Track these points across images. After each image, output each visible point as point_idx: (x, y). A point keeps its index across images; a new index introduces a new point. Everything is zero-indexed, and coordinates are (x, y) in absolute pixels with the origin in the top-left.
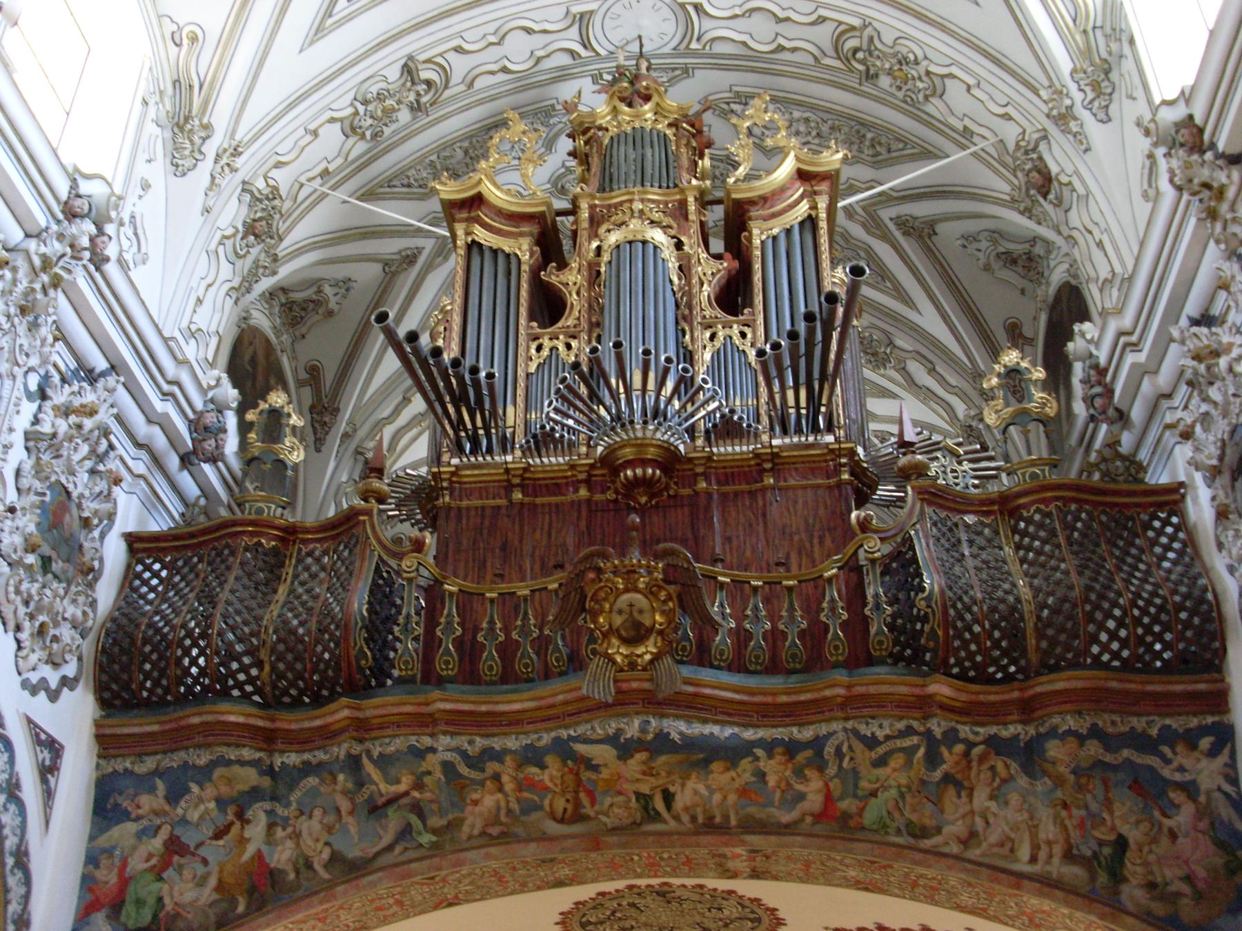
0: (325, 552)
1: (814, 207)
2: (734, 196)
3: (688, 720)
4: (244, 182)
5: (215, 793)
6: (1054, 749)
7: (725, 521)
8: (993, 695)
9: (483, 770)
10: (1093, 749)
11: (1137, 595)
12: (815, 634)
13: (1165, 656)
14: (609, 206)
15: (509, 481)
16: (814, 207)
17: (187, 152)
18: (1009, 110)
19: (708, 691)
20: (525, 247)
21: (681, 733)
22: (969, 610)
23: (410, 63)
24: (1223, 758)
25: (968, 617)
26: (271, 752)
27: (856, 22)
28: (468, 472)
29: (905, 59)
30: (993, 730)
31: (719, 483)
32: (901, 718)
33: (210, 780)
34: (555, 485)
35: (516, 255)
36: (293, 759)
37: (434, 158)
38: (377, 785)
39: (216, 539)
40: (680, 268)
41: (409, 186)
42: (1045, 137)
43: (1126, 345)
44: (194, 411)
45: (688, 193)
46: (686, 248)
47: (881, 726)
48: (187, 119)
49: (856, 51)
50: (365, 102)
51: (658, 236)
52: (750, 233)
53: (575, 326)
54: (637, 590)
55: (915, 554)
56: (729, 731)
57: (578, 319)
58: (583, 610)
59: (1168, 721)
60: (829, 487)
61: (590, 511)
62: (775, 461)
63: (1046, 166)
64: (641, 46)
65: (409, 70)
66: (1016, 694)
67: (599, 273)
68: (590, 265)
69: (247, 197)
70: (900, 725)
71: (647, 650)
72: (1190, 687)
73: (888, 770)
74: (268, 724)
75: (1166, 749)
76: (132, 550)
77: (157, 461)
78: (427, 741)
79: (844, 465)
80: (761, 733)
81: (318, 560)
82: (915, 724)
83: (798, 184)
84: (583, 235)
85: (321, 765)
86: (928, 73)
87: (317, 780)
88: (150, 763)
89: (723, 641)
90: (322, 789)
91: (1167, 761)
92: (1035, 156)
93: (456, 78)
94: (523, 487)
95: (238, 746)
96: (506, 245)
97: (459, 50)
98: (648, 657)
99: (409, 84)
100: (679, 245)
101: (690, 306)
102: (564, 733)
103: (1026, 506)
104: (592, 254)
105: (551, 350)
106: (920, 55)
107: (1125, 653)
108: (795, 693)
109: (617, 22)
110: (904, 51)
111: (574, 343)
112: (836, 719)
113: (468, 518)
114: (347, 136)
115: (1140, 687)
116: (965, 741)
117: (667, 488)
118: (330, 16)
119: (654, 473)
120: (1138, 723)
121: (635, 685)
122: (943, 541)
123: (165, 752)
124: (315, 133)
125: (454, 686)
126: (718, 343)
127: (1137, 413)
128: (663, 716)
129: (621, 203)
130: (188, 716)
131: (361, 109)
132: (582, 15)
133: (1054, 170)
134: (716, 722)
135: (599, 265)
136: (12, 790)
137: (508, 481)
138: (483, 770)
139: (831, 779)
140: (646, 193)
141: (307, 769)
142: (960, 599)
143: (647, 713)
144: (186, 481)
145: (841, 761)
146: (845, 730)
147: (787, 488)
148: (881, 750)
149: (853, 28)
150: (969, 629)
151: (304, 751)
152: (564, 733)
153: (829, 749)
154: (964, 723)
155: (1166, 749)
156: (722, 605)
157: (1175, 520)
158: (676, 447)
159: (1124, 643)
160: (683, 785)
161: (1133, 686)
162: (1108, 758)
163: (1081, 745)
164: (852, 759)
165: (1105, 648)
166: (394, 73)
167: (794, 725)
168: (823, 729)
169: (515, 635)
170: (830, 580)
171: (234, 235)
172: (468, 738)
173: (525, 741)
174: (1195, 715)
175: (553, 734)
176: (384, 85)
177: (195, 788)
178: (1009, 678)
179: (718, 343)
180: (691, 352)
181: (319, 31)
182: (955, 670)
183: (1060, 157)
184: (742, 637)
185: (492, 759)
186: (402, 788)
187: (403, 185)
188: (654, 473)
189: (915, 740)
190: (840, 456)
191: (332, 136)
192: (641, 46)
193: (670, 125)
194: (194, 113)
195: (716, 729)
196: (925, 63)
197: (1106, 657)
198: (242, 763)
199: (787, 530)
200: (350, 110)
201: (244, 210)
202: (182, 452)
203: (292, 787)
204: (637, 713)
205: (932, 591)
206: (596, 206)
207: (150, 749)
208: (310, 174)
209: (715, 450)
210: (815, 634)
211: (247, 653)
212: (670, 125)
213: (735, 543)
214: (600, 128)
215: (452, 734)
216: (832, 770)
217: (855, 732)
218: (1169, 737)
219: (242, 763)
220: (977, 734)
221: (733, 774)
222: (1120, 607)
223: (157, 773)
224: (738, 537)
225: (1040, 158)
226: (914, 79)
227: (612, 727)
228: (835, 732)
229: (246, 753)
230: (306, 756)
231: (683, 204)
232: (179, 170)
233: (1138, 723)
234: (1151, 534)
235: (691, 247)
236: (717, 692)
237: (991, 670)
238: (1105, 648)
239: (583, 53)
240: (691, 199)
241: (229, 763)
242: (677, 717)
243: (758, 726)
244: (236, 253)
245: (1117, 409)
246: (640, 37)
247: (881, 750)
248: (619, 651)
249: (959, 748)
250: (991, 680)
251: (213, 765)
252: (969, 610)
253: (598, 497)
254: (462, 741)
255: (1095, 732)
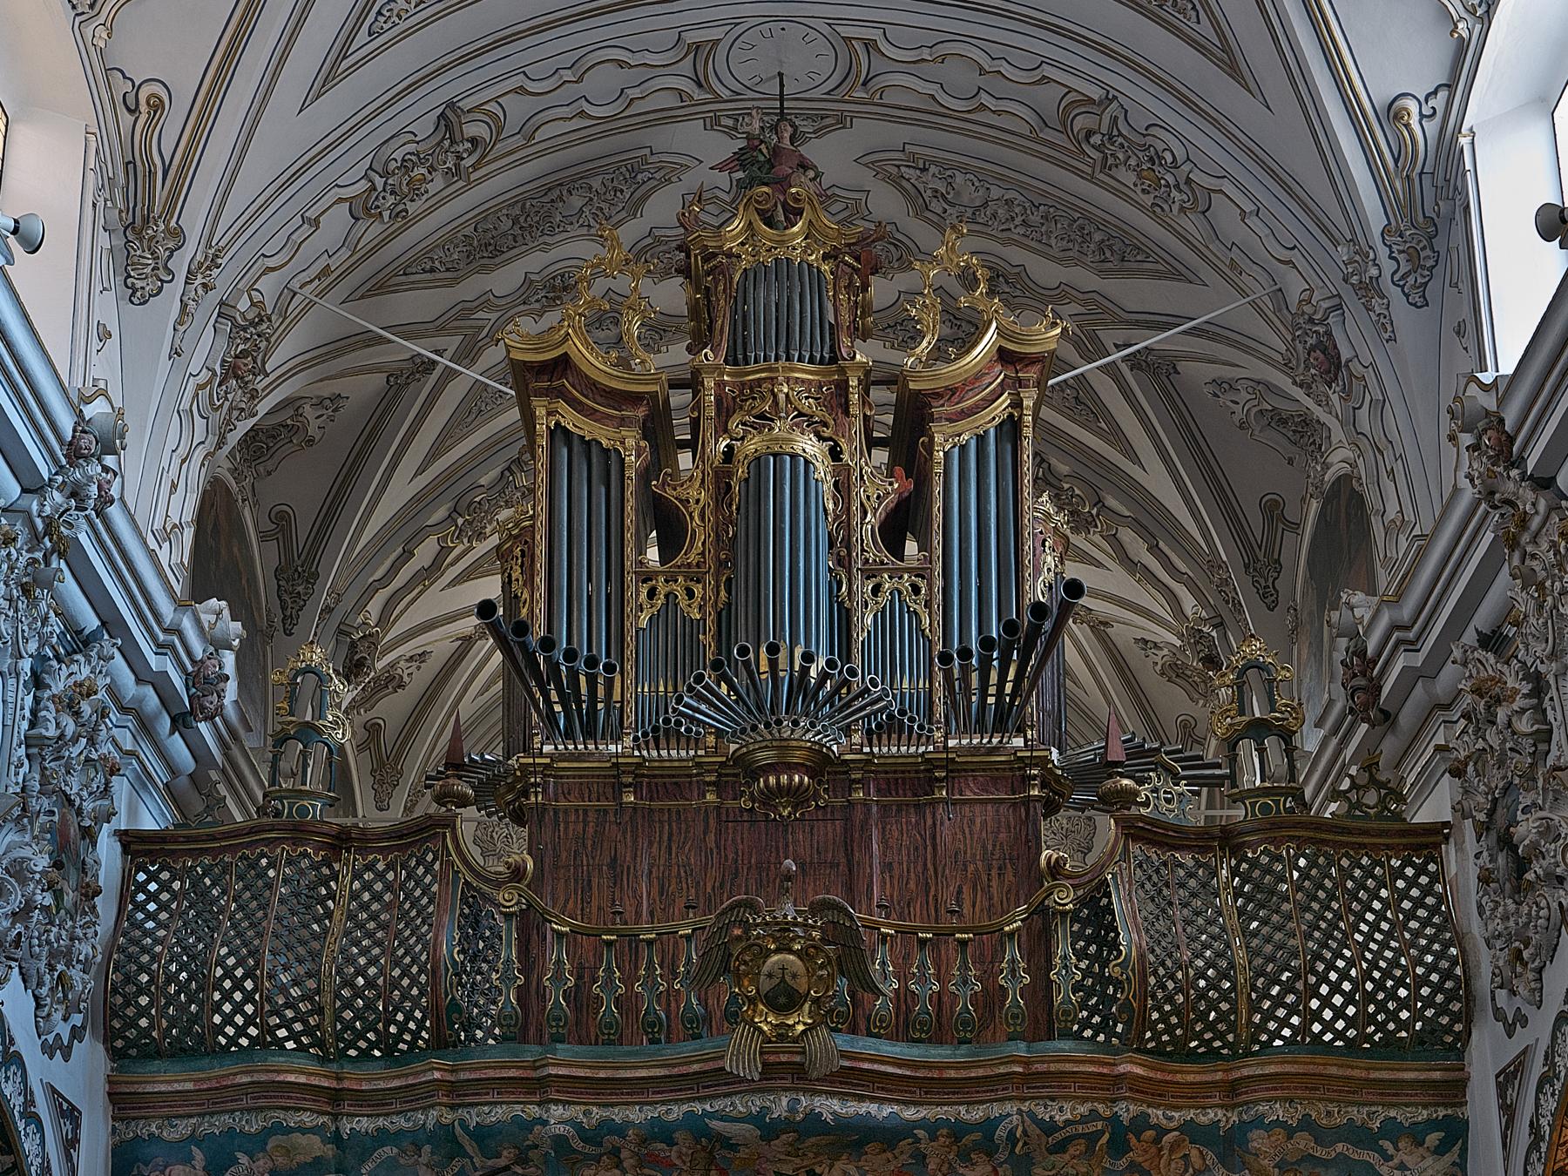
0: (390, 867)
1: (1017, 404)
2: (912, 386)
3: (843, 1097)
4: (222, 303)
5: (270, 1164)
6: (1258, 1140)
7: (884, 842)
8: (1191, 1075)
9: (600, 1144)
10: (1303, 1141)
11: (1374, 965)
12: (991, 999)
13: (1376, 1038)
14: (743, 384)
15: (616, 775)
16: (1017, 404)
17: (148, 270)
18: (1295, 256)
19: (866, 1066)
20: (630, 442)
21: (834, 1113)
22: (1172, 977)
23: (449, 113)
24: (1453, 1155)
25: (1170, 985)
26: (336, 1117)
27: (1096, 93)
28: (565, 765)
29: (1161, 158)
30: (1191, 1114)
31: (879, 791)
32: (1084, 1100)
33: (264, 1150)
34: (670, 783)
35: (616, 450)
36: (365, 1124)
37: (469, 231)
38: (471, 1158)
39: (248, 845)
40: (836, 484)
41: (432, 270)
42: (1339, 307)
43: (1407, 628)
44: (193, 662)
45: (849, 373)
46: (845, 457)
47: (1061, 1109)
48: (146, 220)
49: (1089, 134)
50: (386, 174)
51: (809, 446)
52: (932, 439)
53: (698, 565)
54: (791, 951)
55: (1110, 903)
56: (887, 1110)
57: (703, 553)
58: (726, 970)
59: (1392, 1113)
60: (1014, 805)
61: (719, 821)
62: (953, 768)
63: (1335, 347)
64: (782, 85)
65: (448, 119)
66: (1219, 1076)
67: (729, 486)
68: (716, 472)
69: (227, 326)
70: (1083, 1109)
71: (799, 1022)
72: (1423, 1076)
73: (1067, 1157)
74: (334, 1084)
75: (1387, 1145)
76: (126, 849)
77: (145, 727)
78: (534, 1111)
79: (1034, 777)
80: (923, 1112)
81: (381, 876)
82: (1100, 1107)
83: (998, 368)
84: (708, 428)
85: (400, 1133)
86: (1189, 181)
87: (395, 1150)
88: (183, 1128)
89: (884, 1006)
90: (402, 1161)
91: (1388, 1158)
92: (1322, 330)
93: (511, 126)
94: (636, 788)
95: (298, 1109)
96: (603, 435)
97: (520, 90)
98: (800, 1028)
99: (447, 143)
100: (835, 453)
101: (848, 544)
102: (698, 1108)
103: (1253, 846)
104: (720, 457)
105: (667, 596)
106: (1180, 154)
107: (1351, 1033)
108: (964, 1068)
109: (750, 54)
110: (1160, 146)
111: (698, 590)
112: (1010, 1099)
113: (567, 823)
114: (357, 219)
115: (1363, 1074)
116: (1157, 1127)
117: (816, 796)
118: (345, 58)
119: (801, 780)
120: (1357, 1114)
121: (784, 1058)
122: (1148, 886)
123: (202, 1115)
124: (315, 223)
125: (566, 1046)
126: (883, 599)
127: (1406, 718)
128: (815, 1092)
129: (759, 382)
130: (235, 1074)
131: (379, 182)
132: (698, 46)
133: (1345, 354)
134: (873, 1099)
135: (730, 475)
136: (446, 1142)
137: (617, 777)
138: (600, 1144)
139: (1001, 1165)
140: (793, 370)
141: (382, 1137)
142: (1163, 964)
143: (797, 1090)
144: (177, 746)
145: (1014, 1146)
146: (1020, 1112)
147: (965, 802)
148: (1059, 1136)
149: (1091, 101)
150: (1169, 999)
151: (378, 1115)
152: (698, 1108)
153: (1001, 1133)
154: (1158, 1106)
155: (1387, 1145)
156: (883, 963)
157: (1432, 867)
158: (829, 748)
159: (1351, 1021)
160: (831, 1166)
161: (1356, 1073)
162: (1320, 1152)
163: (1290, 1137)
164: (1025, 1144)
165: (1328, 1026)
166: (424, 128)
167: (961, 1104)
168: (996, 1110)
169: (637, 988)
170: (1011, 934)
171: (210, 382)
172: (583, 1108)
173: (651, 1113)
174: (1425, 1106)
175: (685, 1108)
176: (411, 147)
177: (244, 1159)
178: (1213, 1054)
179: (883, 599)
180: (848, 610)
181: (328, 77)
182: (1151, 1045)
183: (1353, 338)
184: (904, 998)
185: (611, 1132)
186: (502, 1162)
187: (424, 271)
188: (801, 780)
189: (1100, 1125)
190: (1031, 766)
191: (337, 221)
192: (782, 85)
193: (825, 257)
194: (157, 210)
195: (873, 1108)
196: (1186, 168)
197: (1328, 1037)
198: (303, 1130)
199: (961, 857)
200: (364, 185)
201: (222, 343)
202: (175, 712)
203: (364, 1156)
204: (786, 1090)
205: (1128, 956)
206: (725, 383)
207: (181, 1111)
208: (304, 277)
209: (876, 750)
210: (991, 999)
211: (303, 998)
212: (825, 257)
213: (896, 872)
214: (729, 255)
215: (565, 1103)
216: (1002, 1156)
217: (1032, 1115)
218: (1392, 1130)
219: (303, 1130)
220: (1171, 1119)
221: (889, 1155)
222: (1350, 980)
223: (192, 1138)
224: (901, 864)
225: (1329, 334)
226: (1168, 186)
227: (756, 1103)
228: (1009, 1115)
229: (307, 1119)
230: (381, 1122)
231: (843, 387)
232: (136, 296)
233: (1357, 1114)
234: (1400, 884)
235: (852, 456)
236: (876, 1067)
237: (1193, 1044)
238: (1328, 1026)
239: (698, 95)
240: (853, 382)
241: (289, 1131)
242: (831, 1094)
243: (921, 1104)
244: (212, 404)
245: (1382, 711)
246: (780, 75)
247: (1059, 1136)
248: (767, 1021)
249: (1150, 1134)
250: (1192, 1056)
251: (267, 1133)
252: (1172, 977)
253: (730, 803)
254: (575, 1112)
255: (1306, 1124)
